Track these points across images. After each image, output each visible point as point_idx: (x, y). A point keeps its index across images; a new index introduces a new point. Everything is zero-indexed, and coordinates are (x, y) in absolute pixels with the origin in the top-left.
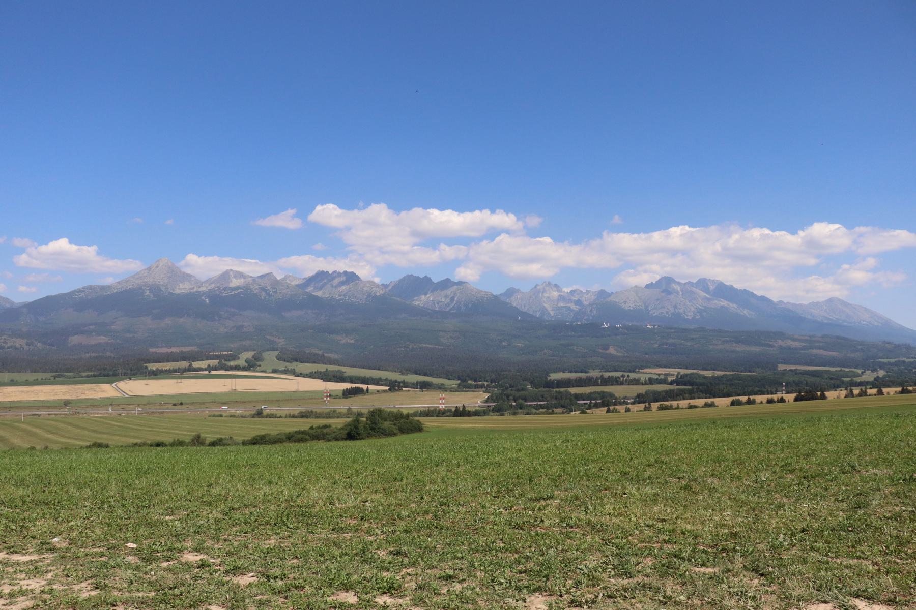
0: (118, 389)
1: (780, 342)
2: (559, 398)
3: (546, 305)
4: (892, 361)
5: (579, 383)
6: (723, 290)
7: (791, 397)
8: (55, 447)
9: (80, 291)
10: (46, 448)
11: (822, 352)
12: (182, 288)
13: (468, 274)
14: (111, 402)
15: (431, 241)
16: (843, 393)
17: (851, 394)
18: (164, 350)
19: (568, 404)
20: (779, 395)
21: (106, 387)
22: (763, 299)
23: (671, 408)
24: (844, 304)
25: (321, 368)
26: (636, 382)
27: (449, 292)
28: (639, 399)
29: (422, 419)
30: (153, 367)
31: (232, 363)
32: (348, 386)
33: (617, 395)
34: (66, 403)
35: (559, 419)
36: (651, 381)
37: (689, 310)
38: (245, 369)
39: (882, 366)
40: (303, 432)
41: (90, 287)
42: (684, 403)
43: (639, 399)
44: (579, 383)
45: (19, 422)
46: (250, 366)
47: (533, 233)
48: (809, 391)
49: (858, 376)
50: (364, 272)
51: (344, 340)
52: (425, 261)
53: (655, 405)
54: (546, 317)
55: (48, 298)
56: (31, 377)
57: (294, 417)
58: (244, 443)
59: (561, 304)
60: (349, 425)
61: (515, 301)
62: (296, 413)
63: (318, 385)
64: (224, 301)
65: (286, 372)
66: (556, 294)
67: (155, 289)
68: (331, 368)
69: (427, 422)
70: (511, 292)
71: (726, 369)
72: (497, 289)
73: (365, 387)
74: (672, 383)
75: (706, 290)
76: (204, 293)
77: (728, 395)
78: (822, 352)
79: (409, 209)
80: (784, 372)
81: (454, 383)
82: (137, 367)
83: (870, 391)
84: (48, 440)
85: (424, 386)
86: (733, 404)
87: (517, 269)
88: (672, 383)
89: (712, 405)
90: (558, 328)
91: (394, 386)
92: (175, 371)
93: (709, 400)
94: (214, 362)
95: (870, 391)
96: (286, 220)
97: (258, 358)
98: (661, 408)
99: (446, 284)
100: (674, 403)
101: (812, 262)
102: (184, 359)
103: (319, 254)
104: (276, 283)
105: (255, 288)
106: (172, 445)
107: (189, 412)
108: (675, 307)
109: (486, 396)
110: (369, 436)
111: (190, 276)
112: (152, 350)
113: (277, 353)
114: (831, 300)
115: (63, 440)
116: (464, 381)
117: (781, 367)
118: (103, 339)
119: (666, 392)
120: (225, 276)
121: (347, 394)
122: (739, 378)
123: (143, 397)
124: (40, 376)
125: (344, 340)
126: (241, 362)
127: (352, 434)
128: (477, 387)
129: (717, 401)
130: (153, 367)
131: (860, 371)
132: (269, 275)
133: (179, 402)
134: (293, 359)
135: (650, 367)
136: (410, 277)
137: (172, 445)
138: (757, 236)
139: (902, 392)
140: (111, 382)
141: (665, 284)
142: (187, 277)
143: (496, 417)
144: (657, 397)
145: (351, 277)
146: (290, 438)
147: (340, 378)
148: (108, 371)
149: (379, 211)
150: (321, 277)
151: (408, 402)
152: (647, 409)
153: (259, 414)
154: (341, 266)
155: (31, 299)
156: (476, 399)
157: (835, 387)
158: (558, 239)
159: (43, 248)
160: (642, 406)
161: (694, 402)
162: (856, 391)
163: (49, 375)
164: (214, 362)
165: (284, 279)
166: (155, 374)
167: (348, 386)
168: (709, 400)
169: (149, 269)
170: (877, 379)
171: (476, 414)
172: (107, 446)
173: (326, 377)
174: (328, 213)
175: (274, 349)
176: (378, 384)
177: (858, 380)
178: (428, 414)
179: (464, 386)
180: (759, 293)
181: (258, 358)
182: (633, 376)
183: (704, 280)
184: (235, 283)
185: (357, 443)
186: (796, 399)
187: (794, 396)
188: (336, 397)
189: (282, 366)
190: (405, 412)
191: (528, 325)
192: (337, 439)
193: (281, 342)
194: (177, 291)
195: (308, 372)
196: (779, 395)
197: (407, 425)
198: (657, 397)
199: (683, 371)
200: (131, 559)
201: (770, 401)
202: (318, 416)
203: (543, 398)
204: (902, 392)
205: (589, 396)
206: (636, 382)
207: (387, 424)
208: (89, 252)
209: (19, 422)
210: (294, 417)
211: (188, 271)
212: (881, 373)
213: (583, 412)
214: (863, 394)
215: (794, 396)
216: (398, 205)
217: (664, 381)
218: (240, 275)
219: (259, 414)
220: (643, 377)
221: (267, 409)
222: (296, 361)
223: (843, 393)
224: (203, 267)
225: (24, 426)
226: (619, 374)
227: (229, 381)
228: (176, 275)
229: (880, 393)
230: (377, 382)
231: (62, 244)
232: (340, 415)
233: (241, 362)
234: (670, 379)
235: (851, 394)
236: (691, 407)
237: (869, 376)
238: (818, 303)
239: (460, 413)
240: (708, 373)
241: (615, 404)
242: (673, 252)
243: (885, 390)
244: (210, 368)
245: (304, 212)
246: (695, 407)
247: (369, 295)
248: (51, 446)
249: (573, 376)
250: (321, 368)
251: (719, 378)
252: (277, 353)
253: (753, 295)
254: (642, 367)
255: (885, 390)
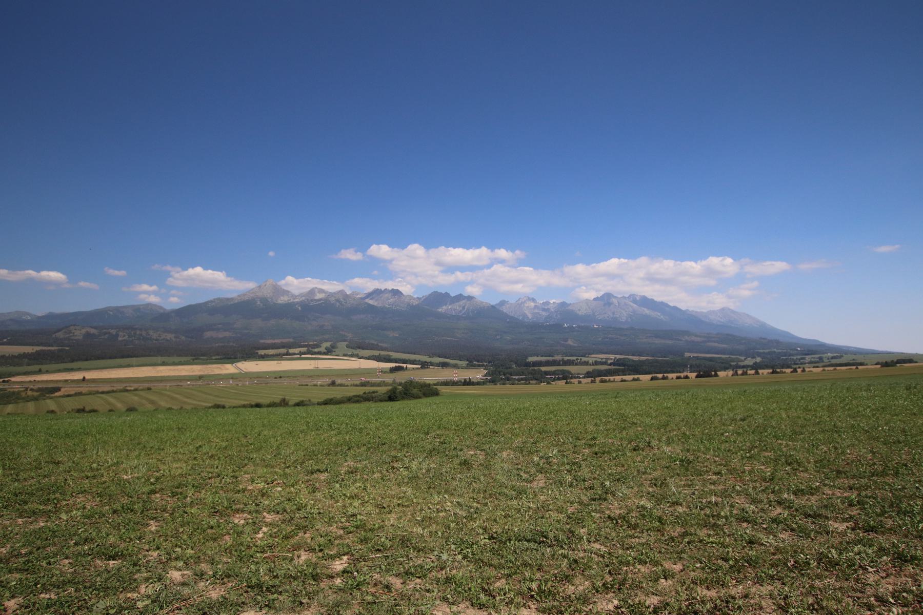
0: (238, 368)
1: (687, 338)
2: (533, 373)
3: (526, 312)
4: (767, 351)
5: (548, 364)
6: (646, 302)
7: (694, 375)
8: (189, 407)
9: (211, 301)
10: (181, 408)
11: (716, 344)
12: (283, 300)
13: (471, 290)
14: (232, 377)
15: (450, 269)
16: (730, 373)
17: (736, 374)
18: (270, 341)
19: (540, 377)
20: (685, 374)
21: (229, 366)
22: (675, 308)
23: (609, 381)
24: (733, 311)
25: (376, 353)
26: (586, 363)
27: (462, 303)
28: (588, 375)
29: (439, 387)
30: (262, 352)
31: (316, 350)
32: (394, 365)
33: (573, 372)
34: (201, 377)
35: (534, 388)
36: (596, 363)
37: (623, 316)
38: (325, 354)
39: (759, 355)
40: (358, 396)
41: (219, 299)
42: (618, 378)
43: (588, 375)
44: (548, 364)
45: (166, 390)
46: (329, 351)
47: (521, 263)
48: (706, 371)
49: (742, 361)
50: (406, 289)
51: (391, 334)
52: (445, 282)
53: (598, 379)
54: (526, 320)
55: (190, 306)
56: (177, 359)
57: (357, 386)
58: (319, 404)
59: (536, 311)
60: (390, 391)
61: (505, 309)
62: (358, 383)
63: (373, 364)
64: (311, 308)
65: (352, 356)
66: (533, 304)
67: (264, 300)
68: (383, 353)
69: (443, 389)
70: (503, 303)
71: (647, 355)
72: (493, 302)
73: (404, 365)
74: (610, 364)
75: (635, 301)
76: (298, 303)
77: (649, 373)
78: (716, 344)
79: (437, 247)
80: (689, 358)
81: (464, 363)
82: (250, 354)
83: (749, 372)
84: (185, 403)
85: (444, 365)
86: (652, 379)
87: (505, 288)
88: (610, 364)
89: (638, 380)
90: (534, 327)
91: (424, 365)
92: (277, 355)
93: (636, 377)
94: (304, 349)
95: (749, 372)
96: (350, 255)
97: (333, 347)
98: (602, 381)
99: (460, 297)
100: (612, 378)
101: (712, 282)
102: (283, 347)
103: (374, 278)
104: (346, 296)
105: (332, 300)
106: (269, 406)
107: (285, 382)
108: (613, 313)
109: (485, 372)
110: (403, 398)
111: (288, 292)
112: (262, 341)
113: (346, 343)
114: (723, 309)
115: (195, 402)
116: (471, 362)
117: (687, 355)
118: (227, 334)
119: (606, 370)
120: (312, 292)
121: (393, 370)
122: (657, 361)
123: (254, 373)
124: (183, 359)
125: (391, 334)
126: (323, 349)
127: (392, 397)
128: (479, 366)
129: (641, 377)
130: (262, 352)
131: (743, 358)
132: (341, 292)
133: (279, 376)
134: (358, 347)
135: (597, 353)
136: (436, 292)
137: (269, 406)
138: (666, 266)
139: (773, 373)
140: (232, 363)
141: (607, 299)
142: (287, 292)
143: (491, 386)
144: (600, 374)
145: (396, 293)
146: (350, 400)
147: (388, 360)
148: (230, 356)
149: (416, 249)
150: (377, 292)
151: (430, 377)
152: (593, 382)
153: (333, 383)
154: (390, 285)
155: (177, 307)
156: (478, 375)
157: (725, 369)
158: (536, 267)
159: (186, 273)
160: (589, 380)
161: (625, 377)
162: (740, 372)
163: (189, 358)
164: (304, 349)
165: (353, 294)
166: (263, 358)
167: (394, 365)
168: (636, 377)
169: (260, 287)
170: (755, 363)
171: (478, 384)
172: (224, 407)
173: (379, 359)
174: (382, 251)
175: (345, 341)
176: (413, 364)
177: (742, 364)
178: (446, 383)
179: (471, 366)
180: (671, 304)
181: (333, 347)
182: (584, 359)
183: (634, 295)
184: (319, 296)
185: (397, 403)
186: (697, 377)
187: (695, 374)
188: (385, 372)
189: (350, 352)
190: (428, 382)
191: (513, 324)
192: (381, 401)
193: (349, 336)
194: (279, 302)
195: (367, 355)
196: (685, 374)
197: (428, 391)
198: (600, 374)
199: (618, 357)
200: (433, 557)
201: (678, 378)
202: (373, 385)
203: (523, 374)
204: (773, 373)
205: (554, 373)
206: (586, 363)
207: (415, 391)
208: (220, 276)
209: (166, 390)
210: (357, 386)
211: (289, 289)
212: (758, 359)
213: (548, 383)
214: (744, 373)
215: (695, 374)
216: (429, 245)
217: (605, 363)
218: (321, 291)
219: (333, 383)
220: (591, 360)
221: (339, 381)
222: (359, 348)
223: (730, 373)
224: (297, 286)
225: (168, 393)
226: (574, 358)
227: (313, 362)
228: (279, 291)
229: (757, 373)
230: (413, 362)
231: (199, 270)
232: (386, 384)
233: (323, 349)
234: (609, 362)
235: (736, 374)
236: (623, 381)
237: (749, 361)
238: (713, 311)
239: (468, 383)
240: (636, 358)
241: (571, 378)
242: (611, 276)
243: (760, 371)
244: (301, 353)
245: (363, 248)
246: (625, 381)
247: (409, 305)
248: (185, 407)
249: (544, 359)
250: (376, 353)
251: (640, 361)
252: (346, 343)
253: (667, 305)
254: (590, 354)
255: (760, 371)
